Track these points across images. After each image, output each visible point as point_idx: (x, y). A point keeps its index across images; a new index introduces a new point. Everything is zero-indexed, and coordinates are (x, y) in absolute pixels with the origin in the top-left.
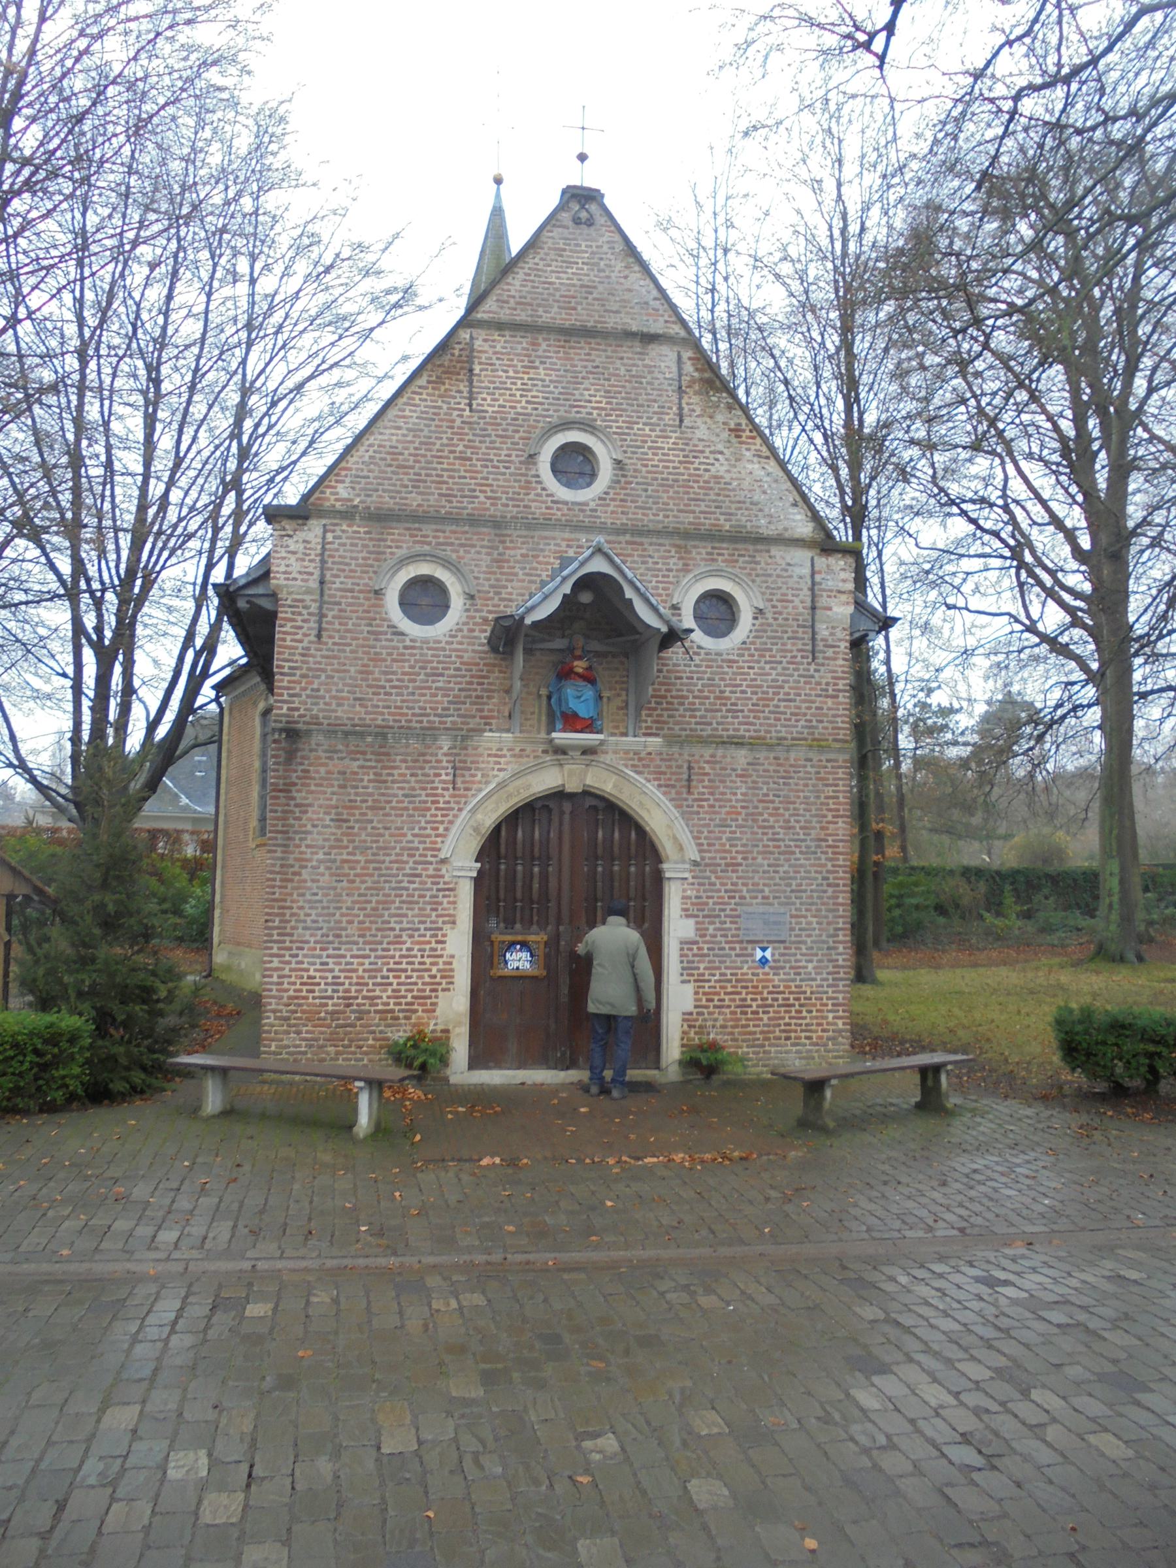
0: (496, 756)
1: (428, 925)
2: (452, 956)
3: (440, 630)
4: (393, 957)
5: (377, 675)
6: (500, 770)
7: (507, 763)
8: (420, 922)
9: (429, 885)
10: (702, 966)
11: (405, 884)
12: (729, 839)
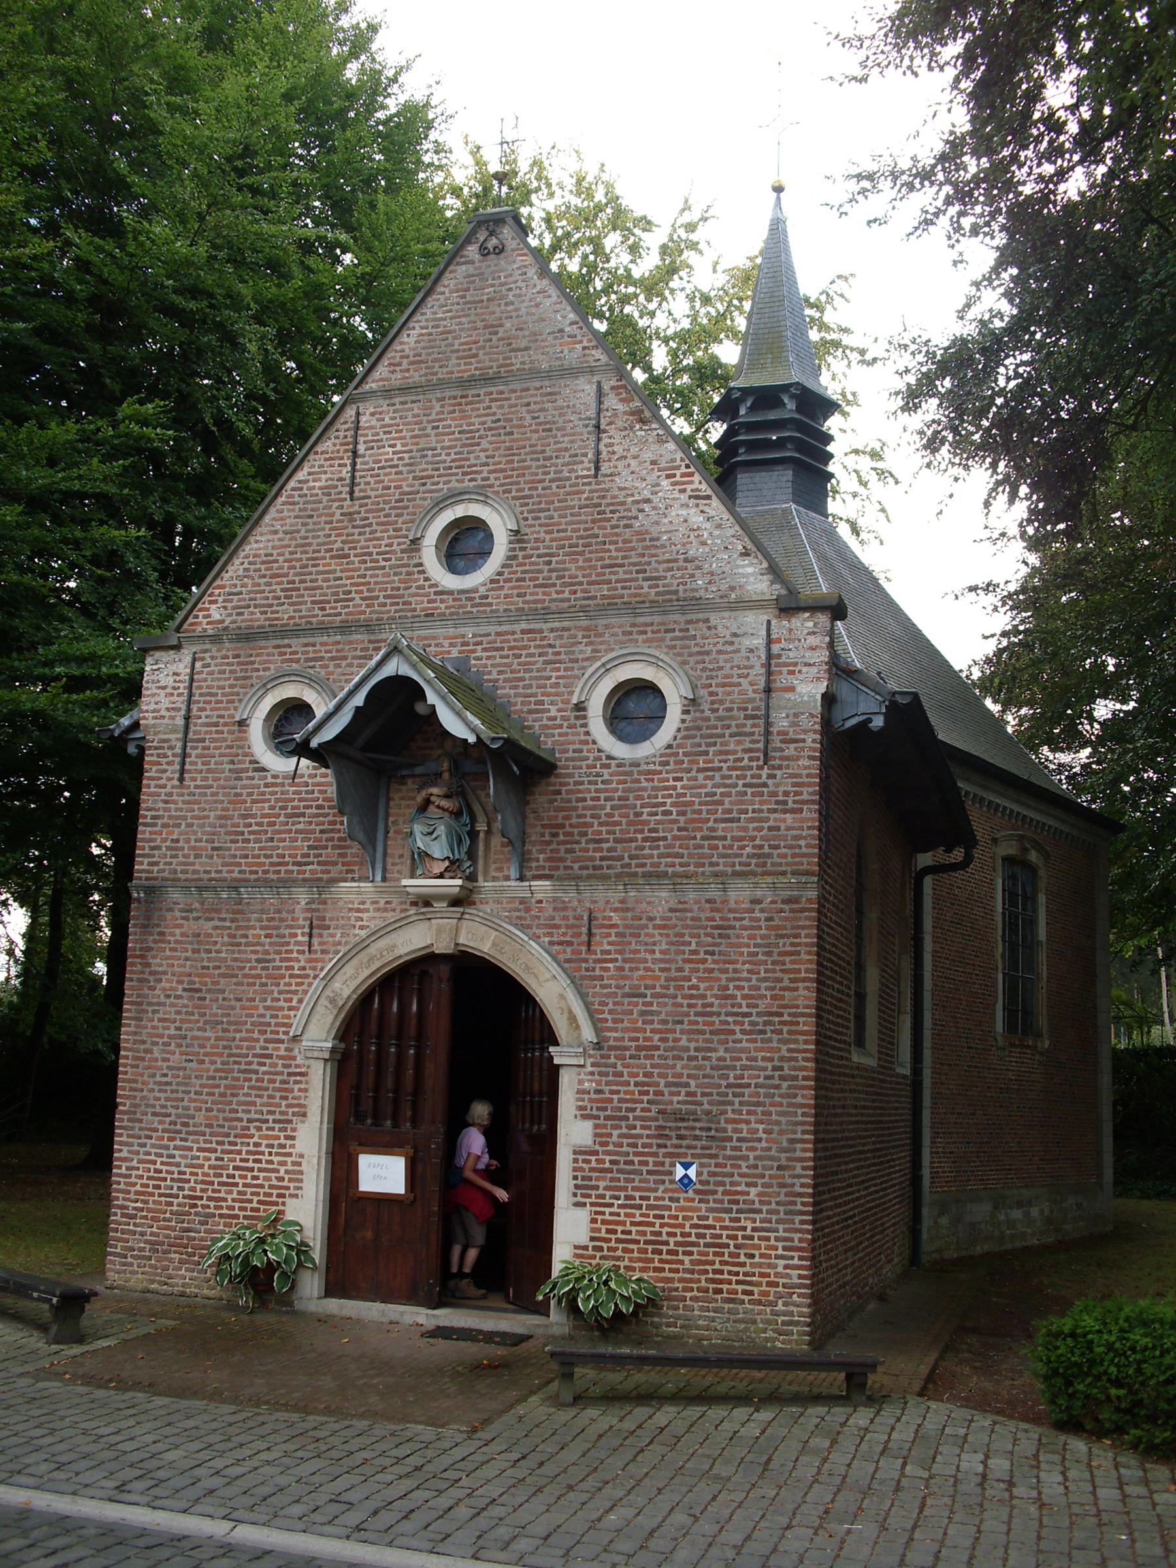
0: (358, 910)
1: (278, 1117)
2: (302, 1156)
4: (239, 1152)
6: (362, 928)
8: (269, 1112)
9: (280, 1068)
10: (602, 1184)
11: (254, 1067)
12: (643, 1013)
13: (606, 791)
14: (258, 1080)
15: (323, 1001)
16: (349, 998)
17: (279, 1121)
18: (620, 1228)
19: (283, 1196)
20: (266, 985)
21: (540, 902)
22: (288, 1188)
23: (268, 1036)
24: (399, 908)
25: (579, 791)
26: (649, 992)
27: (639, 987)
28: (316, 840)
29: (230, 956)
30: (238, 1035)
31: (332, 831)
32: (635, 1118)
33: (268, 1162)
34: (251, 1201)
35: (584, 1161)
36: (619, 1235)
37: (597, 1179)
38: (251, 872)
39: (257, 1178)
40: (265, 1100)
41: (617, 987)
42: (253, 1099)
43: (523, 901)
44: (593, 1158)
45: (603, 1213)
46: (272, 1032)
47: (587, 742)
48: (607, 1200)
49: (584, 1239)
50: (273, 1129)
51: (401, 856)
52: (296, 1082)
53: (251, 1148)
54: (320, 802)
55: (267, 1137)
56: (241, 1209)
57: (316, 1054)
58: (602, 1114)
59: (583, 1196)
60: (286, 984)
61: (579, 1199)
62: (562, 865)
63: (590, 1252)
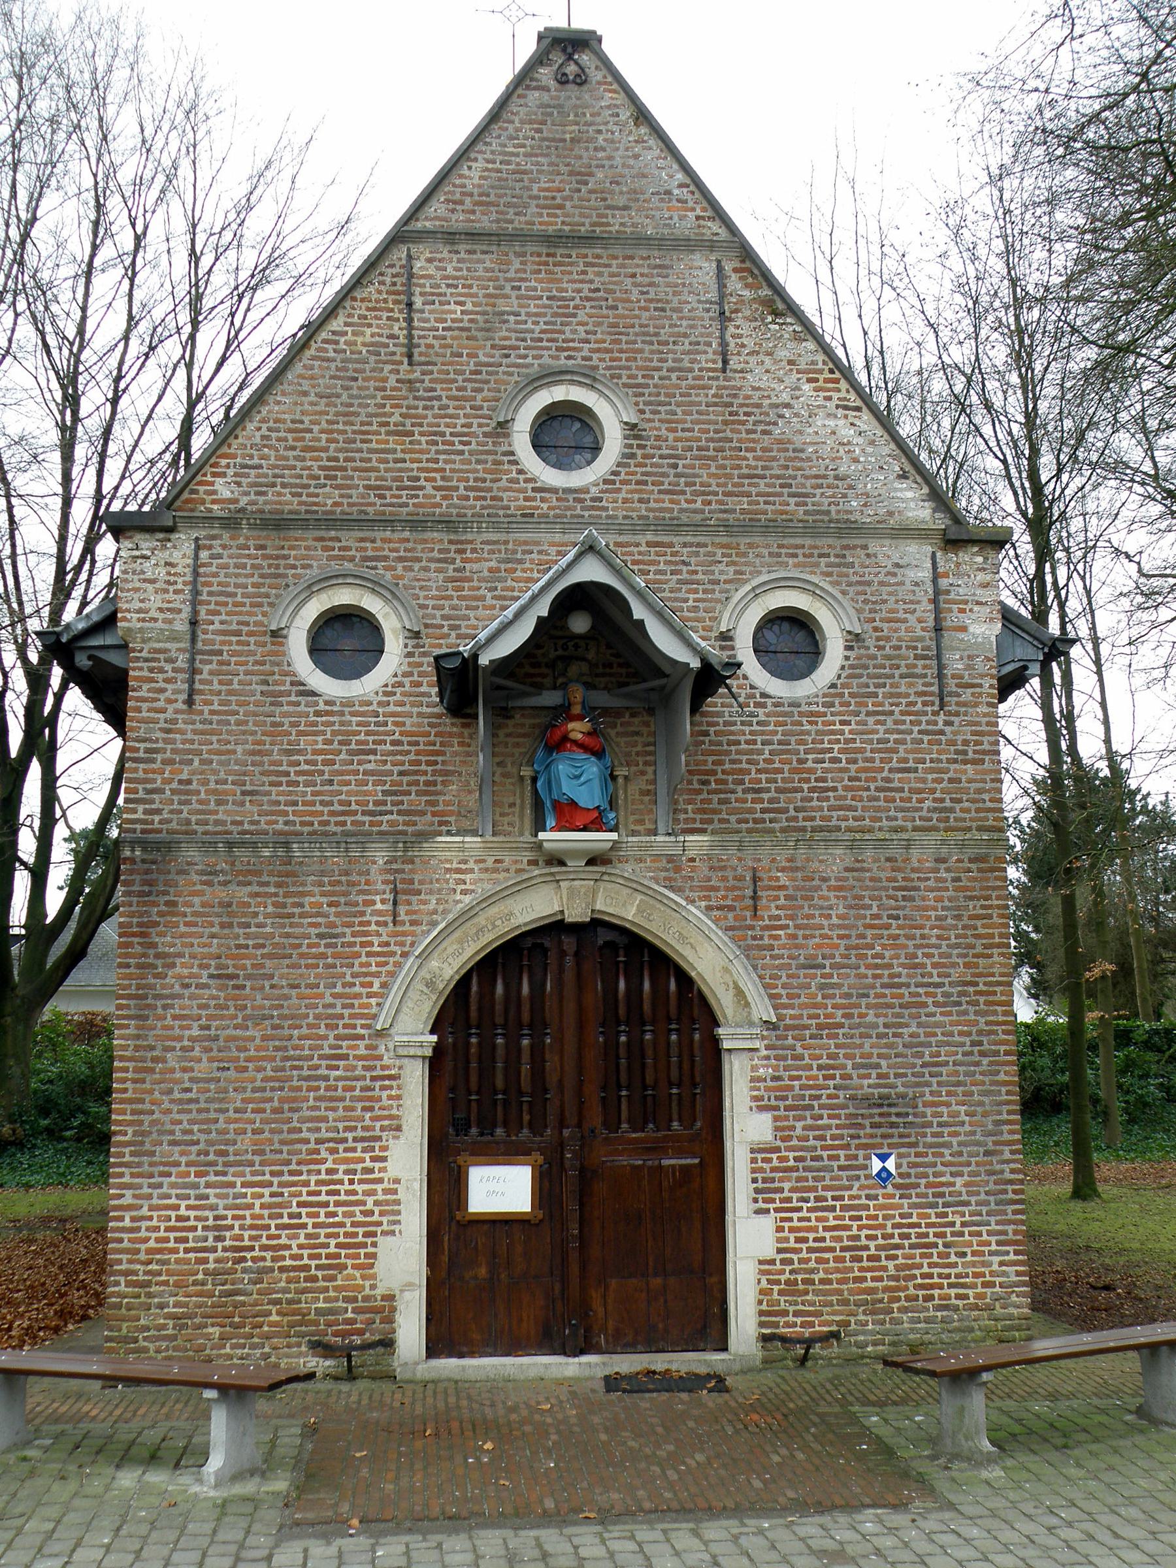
0: (458, 871)
1: (360, 1133)
2: (397, 1181)
4: (306, 1184)
7: (474, 882)
8: (346, 1129)
10: (787, 1186)
11: (323, 1072)
12: (822, 987)
13: (763, 733)
14: (327, 1089)
17: (363, 1139)
18: (811, 1236)
19: (374, 1234)
21: (692, 860)
22: (380, 1224)
23: (341, 1031)
25: (732, 733)
27: (815, 957)
28: (393, 783)
31: (416, 773)
32: (821, 1107)
33: (347, 1193)
35: (764, 1160)
37: (781, 1180)
39: (334, 1214)
40: (341, 1112)
42: (323, 1113)
43: (671, 859)
45: (790, 1220)
46: (345, 1026)
48: (795, 1204)
49: (769, 1252)
50: (354, 1150)
52: (383, 1088)
53: (323, 1176)
54: (397, 737)
55: (346, 1161)
58: (781, 1104)
59: (765, 1201)
60: (362, 965)
63: (778, 1266)
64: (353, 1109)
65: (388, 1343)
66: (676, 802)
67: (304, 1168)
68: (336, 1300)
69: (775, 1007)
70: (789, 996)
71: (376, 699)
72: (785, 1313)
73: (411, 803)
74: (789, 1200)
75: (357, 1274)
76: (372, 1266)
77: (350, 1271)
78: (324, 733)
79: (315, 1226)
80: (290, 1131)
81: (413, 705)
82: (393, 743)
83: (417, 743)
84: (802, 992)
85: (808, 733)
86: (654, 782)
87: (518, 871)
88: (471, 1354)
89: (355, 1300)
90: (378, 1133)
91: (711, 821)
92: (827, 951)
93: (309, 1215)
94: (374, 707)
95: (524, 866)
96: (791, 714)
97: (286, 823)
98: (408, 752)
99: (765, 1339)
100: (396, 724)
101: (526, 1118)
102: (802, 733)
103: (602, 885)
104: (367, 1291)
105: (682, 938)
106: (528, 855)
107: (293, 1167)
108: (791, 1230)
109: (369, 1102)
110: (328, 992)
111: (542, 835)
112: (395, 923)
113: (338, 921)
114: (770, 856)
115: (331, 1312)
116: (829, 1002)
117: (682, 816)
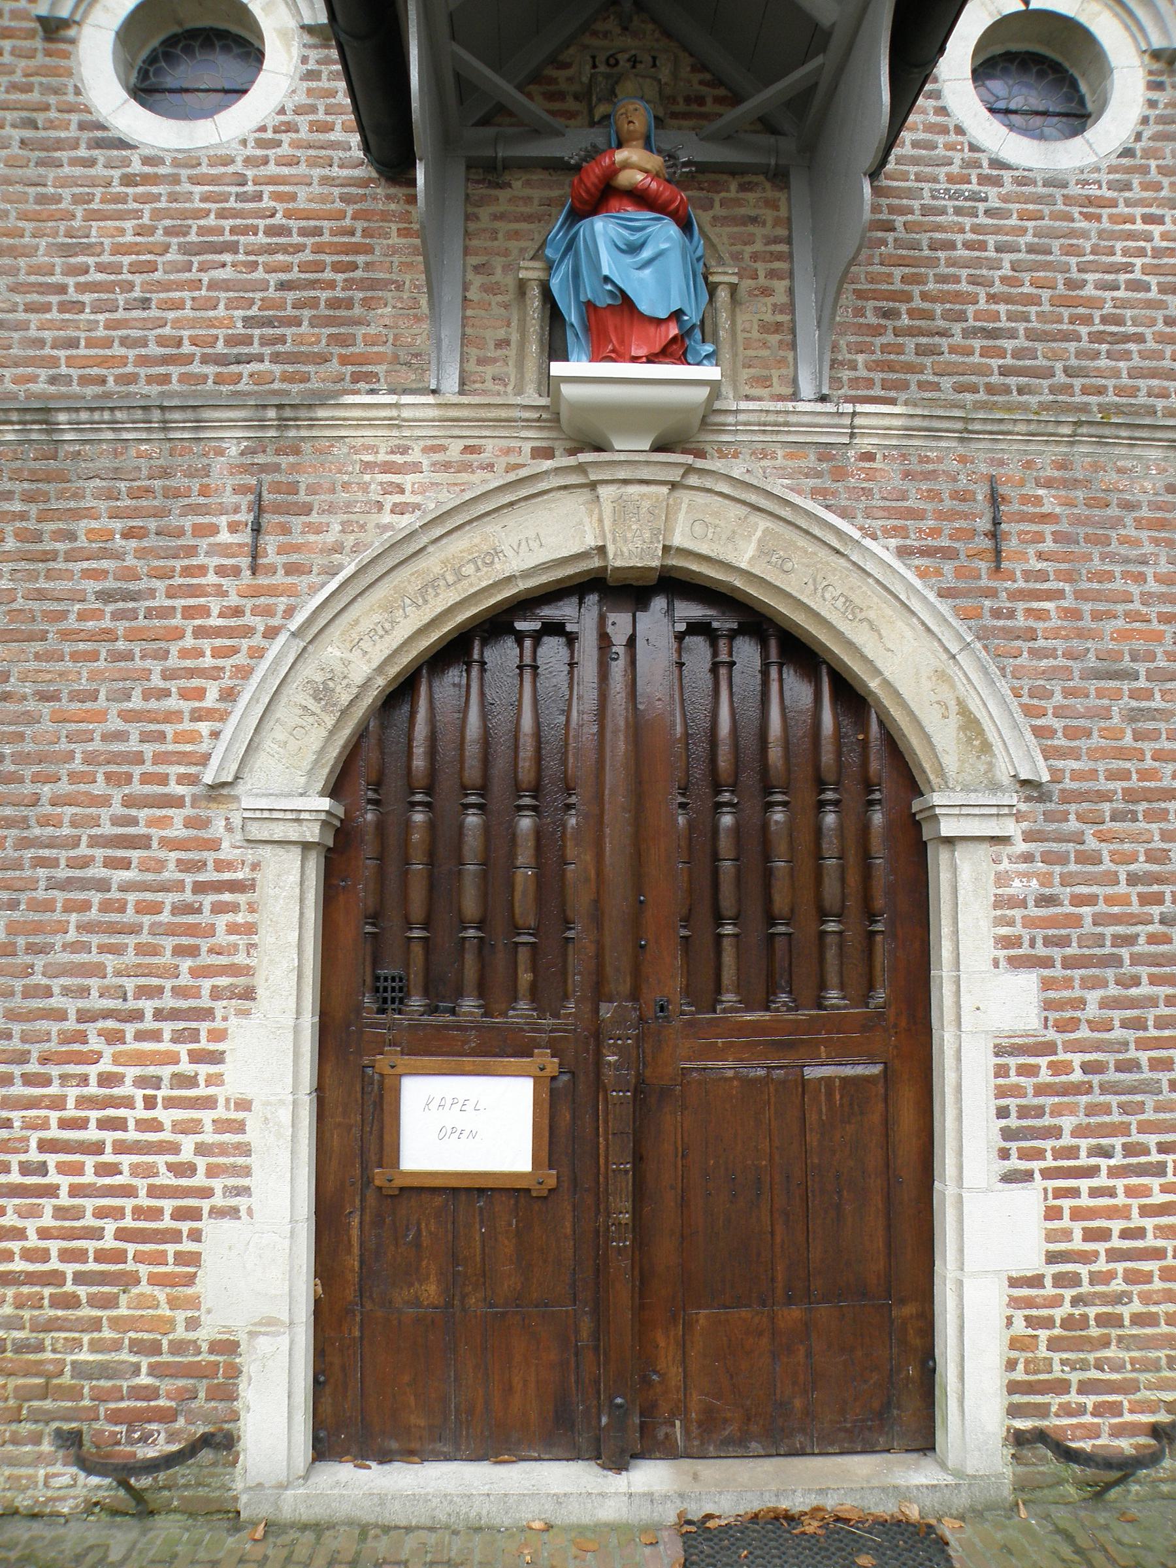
0: (388, 467)
1: (168, 1002)
2: (244, 1105)
3: (233, 125)
4: (58, 1103)
5: (42, 259)
7: (423, 489)
8: (144, 992)
9: (170, 874)
10: (1067, 1123)
11: (97, 871)
12: (1133, 716)
13: (997, 230)
14: (105, 907)
15: (297, 695)
16: (365, 686)
17: (174, 1015)
18: (1116, 1226)
19: (193, 1214)
20: (128, 656)
21: (869, 457)
22: (207, 1193)
23: (136, 788)
24: (501, 463)
25: (938, 228)
26: (1142, 668)
27: (1117, 656)
28: (266, 304)
29: (23, 587)
30: (47, 790)
31: (312, 285)
32: (1136, 960)
33: (142, 1125)
34: (97, 1234)
35: (1023, 1070)
36: (1116, 1243)
37: (1057, 1112)
38: (84, 380)
39: (114, 1170)
40: (130, 958)
41: (1069, 655)
42: (94, 957)
43: (825, 452)
44: (1043, 1061)
45: (1074, 1193)
46: (146, 779)
47: (944, 130)
48: (1084, 1161)
49: (1032, 1262)
50: (156, 1036)
51: (503, 343)
52: (218, 909)
53: (93, 1089)
54: (278, 219)
55: (140, 1059)
56: (67, 1256)
57: (279, 831)
58: (1057, 953)
59: (1024, 1155)
60: (184, 654)
61: (1015, 1163)
62: (913, 378)
63: (1049, 1290)
64: (155, 951)
65: (221, 1442)
66: (835, 348)
67: (54, 1071)
68: (116, 1346)
69: (1047, 754)
70: (1071, 733)
71: (241, 153)
72: (1061, 1387)
73: (299, 340)
74: (1072, 1152)
75: (161, 1294)
76: (190, 1280)
77: (144, 1288)
78: (137, 214)
79: (75, 1191)
80: (28, 993)
81: (313, 163)
82: (270, 231)
83: (318, 232)
84: (1096, 726)
85: (1084, 234)
86: (791, 308)
87: (511, 468)
88: (412, 1454)
89: (154, 1348)
90: (205, 1002)
91: (905, 386)
92: (1139, 645)
93: (62, 1169)
94: (238, 167)
95: (526, 457)
96: (1049, 200)
97: (53, 380)
98: (300, 248)
99: (1019, 1439)
100: (277, 197)
101: (525, 977)
102: (1073, 233)
103: (685, 496)
104: (180, 1333)
105: (851, 608)
106: (533, 437)
107: (33, 1067)
108: (1077, 1214)
109: (189, 936)
110: (114, 708)
111: (558, 369)
112: (254, 570)
113: (141, 566)
114: (1022, 461)
115: (104, 1371)
116: (1148, 747)
117: (846, 374)
